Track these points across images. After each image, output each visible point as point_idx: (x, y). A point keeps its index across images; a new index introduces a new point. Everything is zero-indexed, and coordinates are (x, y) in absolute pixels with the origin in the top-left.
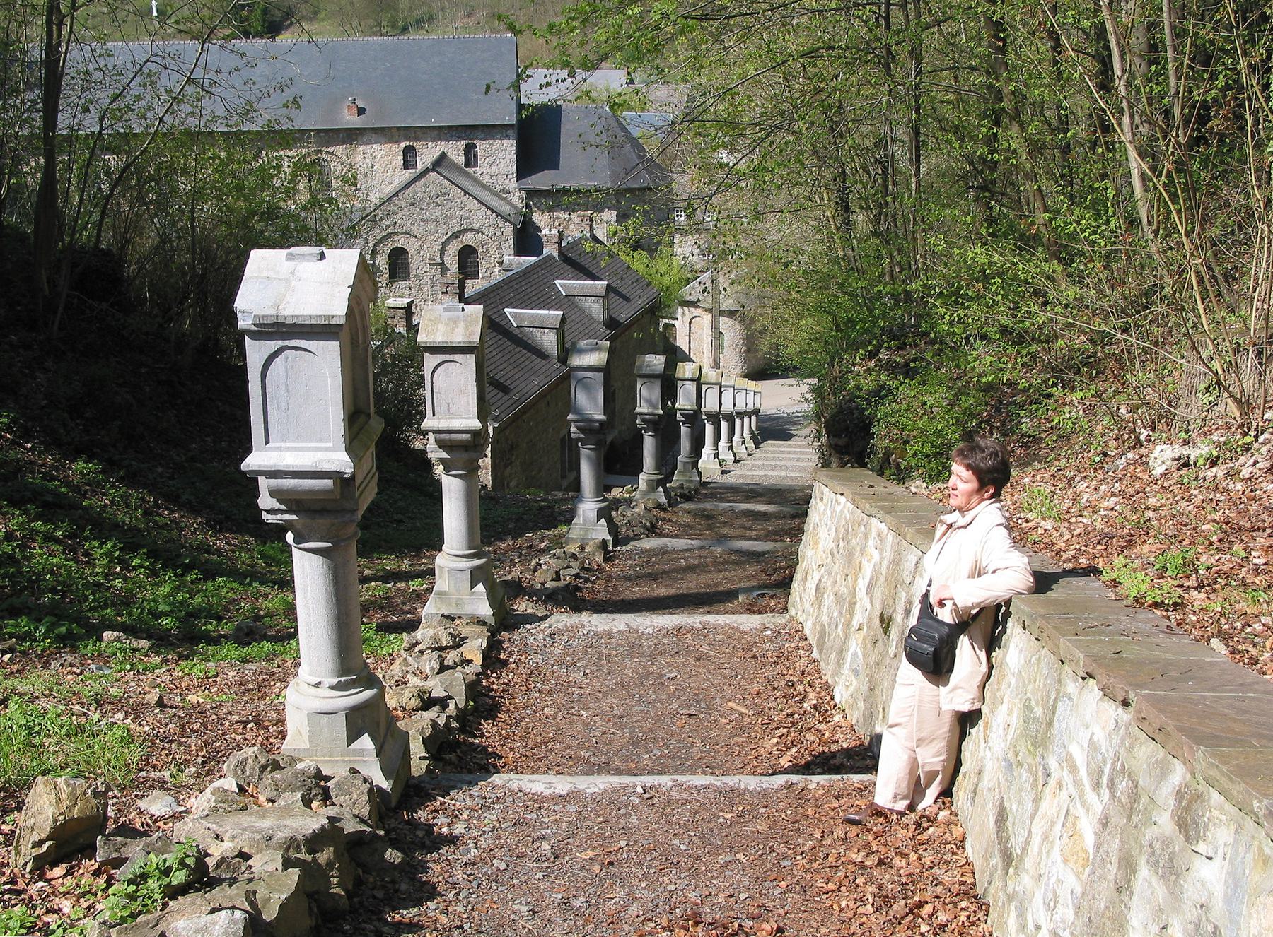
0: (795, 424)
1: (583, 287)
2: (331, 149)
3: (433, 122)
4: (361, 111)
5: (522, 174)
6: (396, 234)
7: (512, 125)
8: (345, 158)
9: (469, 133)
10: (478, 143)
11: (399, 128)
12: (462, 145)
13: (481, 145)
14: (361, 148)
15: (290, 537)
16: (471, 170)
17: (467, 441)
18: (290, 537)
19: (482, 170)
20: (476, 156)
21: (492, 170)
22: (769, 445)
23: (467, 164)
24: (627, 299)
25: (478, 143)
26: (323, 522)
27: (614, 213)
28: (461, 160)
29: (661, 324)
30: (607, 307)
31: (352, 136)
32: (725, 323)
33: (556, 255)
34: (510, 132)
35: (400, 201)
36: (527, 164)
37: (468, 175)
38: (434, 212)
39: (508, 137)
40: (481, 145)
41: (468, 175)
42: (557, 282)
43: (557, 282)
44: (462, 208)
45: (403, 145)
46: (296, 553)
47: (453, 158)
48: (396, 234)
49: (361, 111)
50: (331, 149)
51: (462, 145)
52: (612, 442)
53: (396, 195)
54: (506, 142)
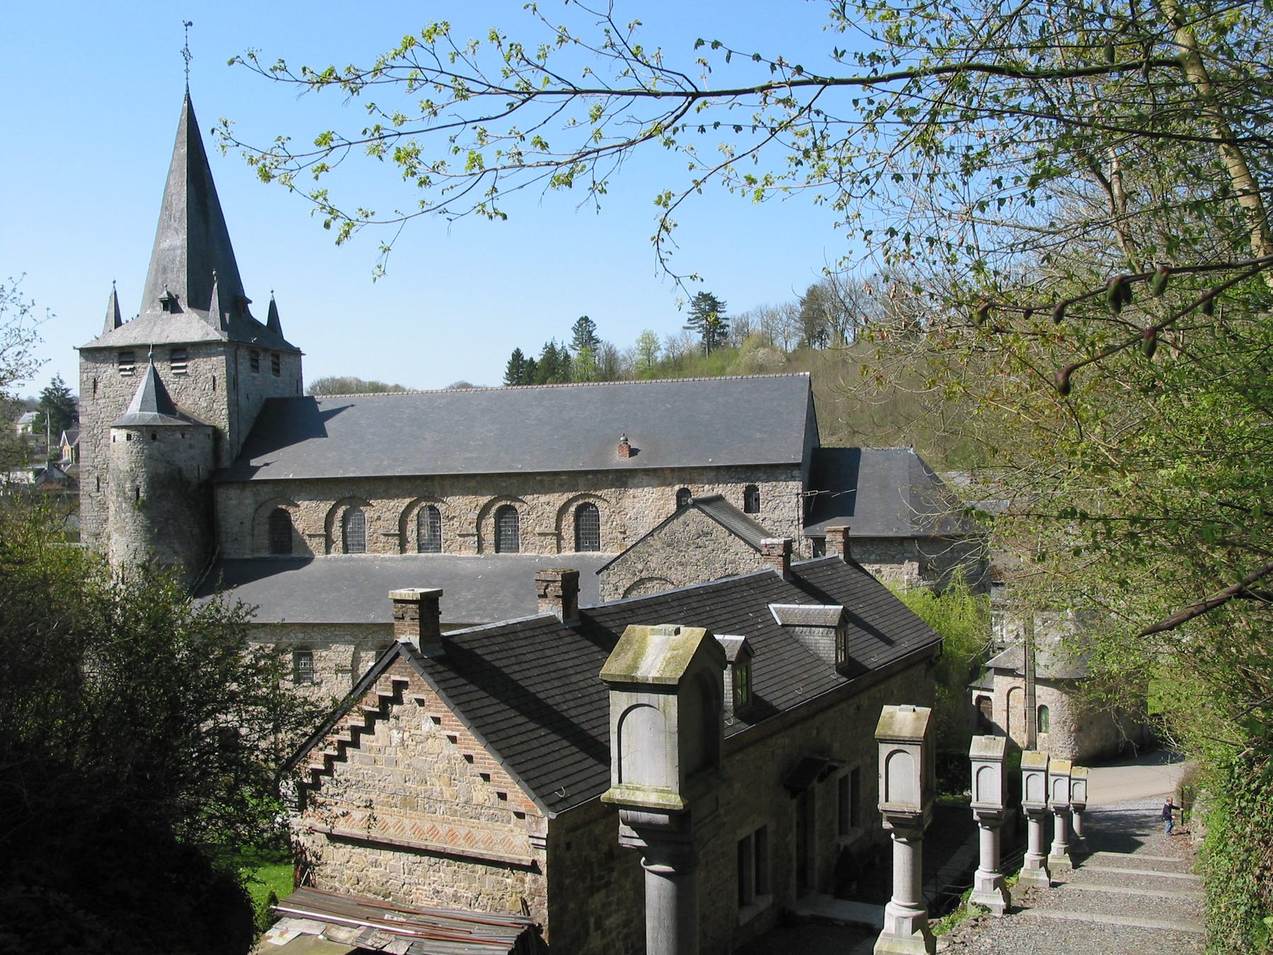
0: (1142, 825)
1: (808, 613)
2: (599, 493)
3: (710, 462)
4: (633, 452)
5: (807, 523)
6: (651, 579)
7: (797, 465)
8: (614, 501)
9: (749, 474)
10: (760, 485)
11: (672, 470)
12: (741, 487)
13: (763, 488)
14: (631, 491)
15: (893, 836)
16: (751, 516)
17: (664, 826)
18: (893, 836)
19: (764, 515)
20: (757, 500)
21: (775, 516)
22: (1101, 862)
23: (748, 508)
24: (890, 642)
25: (760, 485)
26: (906, 831)
27: (916, 565)
28: (740, 504)
29: (974, 698)
30: (842, 644)
31: (622, 479)
32: (1045, 695)
33: (780, 572)
34: (796, 473)
35: (656, 542)
36: (814, 512)
37: (746, 520)
38: (694, 554)
39: (793, 478)
40: (763, 488)
41: (746, 520)
42: (772, 606)
43: (772, 606)
44: (726, 551)
45: (677, 488)
46: (895, 843)
47: (732, 502)
48: (651, 579)
49: (633, 452)
50: (599, 493)
51: (741, 487)
52: (846, 847)
53: (651, 534)
54: (791, 484)
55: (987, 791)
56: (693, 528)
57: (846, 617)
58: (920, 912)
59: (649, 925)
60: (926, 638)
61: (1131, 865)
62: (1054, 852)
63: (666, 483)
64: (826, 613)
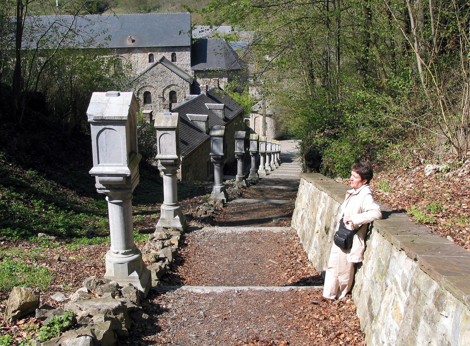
0: (294, 156)
1: (215, 106)
2: (122, 55)
3: (160, 45)
4: (133, 41)
5: (193, 64)
6: (146, 86)
7: (189, 46)
9: (173, 49)
11: (147, 47)
12: (170, 53)
13: (177, 54)
14: (133, 55)
16: (174, 63)
19: (178, 63)
20: (176, 58)
21: (181, 63)
22: (284, 164)
23: (173, 61)
24: (232, 110)
27: (227, 79)
28: (170, 59)
29: (244, 120)
30: (224, 114)
31: (130, 50)
32: (268, 119)
33: (205, 94)
34: (188, 49)
35: (148, 74)
36: (194, 61)
37: (173, 65)
38: (160, 78)
39: (187, 51)
40: (177, 54)
41: (173, 65)
42: (206, 104)
43: (206, 104)
44: (171, 77)
45: (149, 53)
48: (146, 86)
49: (133, 41)
50: (122, 55)
51: (170, 53)
52: (226, 163)
53: (146, 72)
54: (187, 52)
55: (239, 148)
56: (160, 70)
57: (225, 106)
58: (178, 207)
59: (238, 167)
60: (241, 108)
61: (292, 165)
62: (260, 169)
63: (145, 52)
64: (220, 106)
